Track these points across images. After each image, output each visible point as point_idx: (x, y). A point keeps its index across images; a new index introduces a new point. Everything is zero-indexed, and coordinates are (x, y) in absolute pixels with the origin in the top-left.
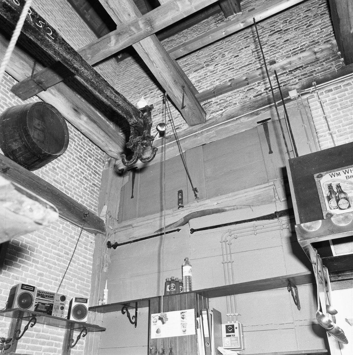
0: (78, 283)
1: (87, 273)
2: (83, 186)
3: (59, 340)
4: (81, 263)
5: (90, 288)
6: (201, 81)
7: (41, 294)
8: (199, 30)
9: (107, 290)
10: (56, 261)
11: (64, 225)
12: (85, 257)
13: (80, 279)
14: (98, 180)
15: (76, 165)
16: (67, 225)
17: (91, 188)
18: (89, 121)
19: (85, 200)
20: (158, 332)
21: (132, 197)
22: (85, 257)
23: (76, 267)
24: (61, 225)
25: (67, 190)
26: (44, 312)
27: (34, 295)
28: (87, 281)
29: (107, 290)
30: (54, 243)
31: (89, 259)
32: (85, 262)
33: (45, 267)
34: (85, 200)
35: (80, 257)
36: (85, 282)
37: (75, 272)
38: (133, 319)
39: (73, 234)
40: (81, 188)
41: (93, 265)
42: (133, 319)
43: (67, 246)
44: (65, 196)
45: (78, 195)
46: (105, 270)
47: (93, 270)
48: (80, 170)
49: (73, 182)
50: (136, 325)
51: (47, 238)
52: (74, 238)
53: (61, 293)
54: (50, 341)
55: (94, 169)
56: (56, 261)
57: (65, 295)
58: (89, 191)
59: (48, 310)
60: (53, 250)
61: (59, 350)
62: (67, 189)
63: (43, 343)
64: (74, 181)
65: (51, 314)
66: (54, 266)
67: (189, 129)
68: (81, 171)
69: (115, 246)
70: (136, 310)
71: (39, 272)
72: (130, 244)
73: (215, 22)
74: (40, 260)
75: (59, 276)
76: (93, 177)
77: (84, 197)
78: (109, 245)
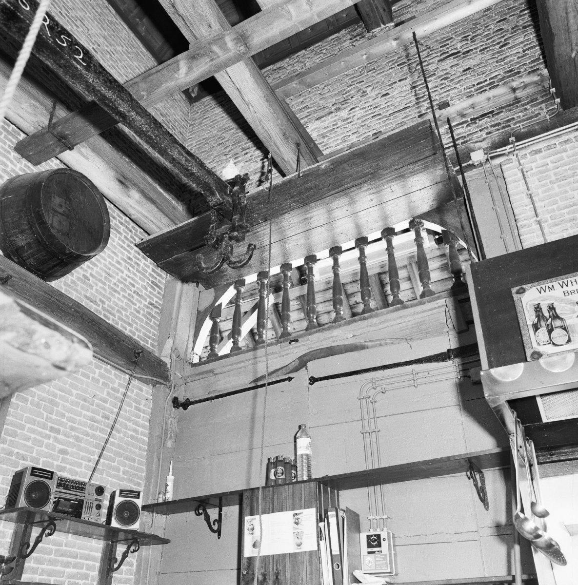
1: (140, 449)
4: (130, 433)
5: (144, 475)
6: (327, 136)
7: (63, 483)
8: (324, 51)
10: (88, 429)
11: (102, 371)
12: (137, 424)
13: (127, 458)
14: (157, 297)
18: (143, 200)
22: (137, 424)
24: (97, 371)
27: (53, 485)
28: (140, 463)
29: (173, 477)
30: (85, 400)
31: (143, 427)
32: (135, 431)
33: (71, 440)
35: (128, 424)
36: (136, 465)
37: (120, 447)
38: (214, 524)
39: (116, 385)
41: (150, 435)
45: (125, 322)
46: (169, 443)
47: (149, 444)
48: (129, 280)
50: (219, 535)
51: (74, 392)
53: (96, 482)
54: (78, 560)
56: (88, 429)
57: (102, 485)
59: (74, 511)
60: (84, 412)
61: (93, 577)
62: (108, 311)
63: (67, 565)
66: (85, 437)
69: (186, 404)
70: (220, 510)
73: (351, 39)
74: (62, 429)
77: (135, 325)
78: (176, 403)
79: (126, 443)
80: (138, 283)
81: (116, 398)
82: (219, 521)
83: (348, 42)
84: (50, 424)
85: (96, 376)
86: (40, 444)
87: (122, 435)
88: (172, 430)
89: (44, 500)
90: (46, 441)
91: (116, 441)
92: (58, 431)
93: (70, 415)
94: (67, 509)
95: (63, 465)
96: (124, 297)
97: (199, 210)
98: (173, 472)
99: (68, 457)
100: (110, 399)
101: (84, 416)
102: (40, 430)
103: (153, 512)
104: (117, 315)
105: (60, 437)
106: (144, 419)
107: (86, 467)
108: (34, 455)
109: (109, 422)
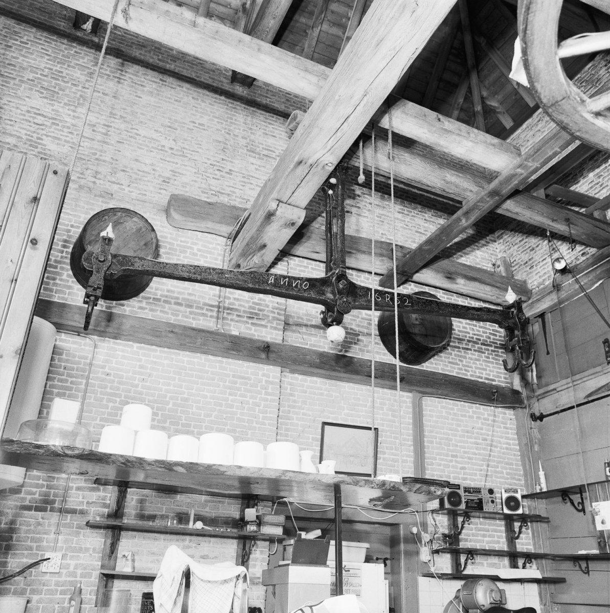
0: (506, 469)
1: (514, 455)
2: (483, 355)
3: (500, 531)
4: (505, 446)
5: (522, 473)
6: (602, 175)
7: (467, 490)
8: (584, 84)
9: (543, 472)
10: (475, 451)
11: (474, 409)
12: (507, 438)
13: (507, 464)
14: (500, 340)
15: (469, 333)
16: (476, 408)
17: (494, 353)
18: (468, 282)
19: (490, 371)
20: (603, 523)
21: (548, 353)
22: (507, 438)
23: (499, 452)
24: (471, 410)
25: (466, 368)
26: (475, 507)
27: (461, 492)
28: (517, 465)
29: (543, 472)
30: (468, 432)
31: (513, 439)
32: (507, 443)
33: (465, 460)
34: (490, 371)
35: (501, 440)
36: (514, 467)
37: (499, 457)
38: (579, 506)
39: (486, 416)
40: (481, 359)
41: (520, 444)
42: (579, 506)
43: (484, 431)
44: (465, 381)
45: (480, 369)
46: (536, 448)
47: (520, 450)
48: (475, 337)
49: (470, 356)
50: (584, 512)
51: (459, 429)
52: (488, 420)
53: (489, 485)
54: (490, 533)
55: (491, 328)
56: (475, 451)
57: (492, 488)
58: (493, 358)
59: (478, 506)
60: (470, 440)
61: (503, 542)
62: (467, 366)
63: (484, 536)
64: (472, 354)
65: (483, 509)
66: (474, 456)
67: (597, 254)
68: (476, 339)
69: (541, 417)
70: (581, 495)
71: (461, 465)
72: (557, 415)
73: (606, 66)
74: (458, 454)
75: (482, 465)
76: (494, 339)
77: (488, 368)
78: (534, 418)
79: (503, 454)
80: (482, 336)
81: (488, 425)
82: (582, 503)
83: (604, 69)
84: (450, 453)
85: (471, 414)
86: (448, 466)
87: (499, 449)
88: (536, 438)
89: (460, 503)
90: (451, 464)
91: (496, 454)
92: (456, 456)
93: (461, 444)
94: (473, 505)
95: (465, 476)
96: (475, 350)
97: (514, 260)
98: (543, 468)
99: (467, 471)
100: (484, 427)
101: (470, 442)
102: (446, 458)
103: (534, 498)
104: (474, 366)
105: (458, 459)
106: (512, 434)
107: (481, 475)
108: (446, 474)
109: (488, 442)
